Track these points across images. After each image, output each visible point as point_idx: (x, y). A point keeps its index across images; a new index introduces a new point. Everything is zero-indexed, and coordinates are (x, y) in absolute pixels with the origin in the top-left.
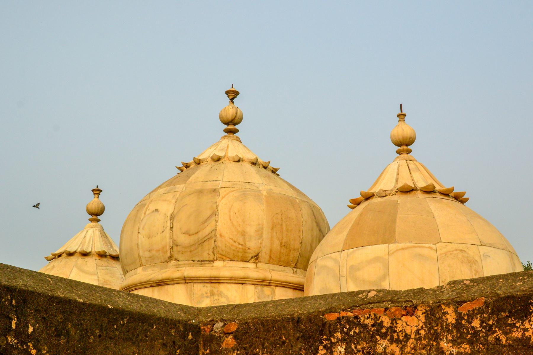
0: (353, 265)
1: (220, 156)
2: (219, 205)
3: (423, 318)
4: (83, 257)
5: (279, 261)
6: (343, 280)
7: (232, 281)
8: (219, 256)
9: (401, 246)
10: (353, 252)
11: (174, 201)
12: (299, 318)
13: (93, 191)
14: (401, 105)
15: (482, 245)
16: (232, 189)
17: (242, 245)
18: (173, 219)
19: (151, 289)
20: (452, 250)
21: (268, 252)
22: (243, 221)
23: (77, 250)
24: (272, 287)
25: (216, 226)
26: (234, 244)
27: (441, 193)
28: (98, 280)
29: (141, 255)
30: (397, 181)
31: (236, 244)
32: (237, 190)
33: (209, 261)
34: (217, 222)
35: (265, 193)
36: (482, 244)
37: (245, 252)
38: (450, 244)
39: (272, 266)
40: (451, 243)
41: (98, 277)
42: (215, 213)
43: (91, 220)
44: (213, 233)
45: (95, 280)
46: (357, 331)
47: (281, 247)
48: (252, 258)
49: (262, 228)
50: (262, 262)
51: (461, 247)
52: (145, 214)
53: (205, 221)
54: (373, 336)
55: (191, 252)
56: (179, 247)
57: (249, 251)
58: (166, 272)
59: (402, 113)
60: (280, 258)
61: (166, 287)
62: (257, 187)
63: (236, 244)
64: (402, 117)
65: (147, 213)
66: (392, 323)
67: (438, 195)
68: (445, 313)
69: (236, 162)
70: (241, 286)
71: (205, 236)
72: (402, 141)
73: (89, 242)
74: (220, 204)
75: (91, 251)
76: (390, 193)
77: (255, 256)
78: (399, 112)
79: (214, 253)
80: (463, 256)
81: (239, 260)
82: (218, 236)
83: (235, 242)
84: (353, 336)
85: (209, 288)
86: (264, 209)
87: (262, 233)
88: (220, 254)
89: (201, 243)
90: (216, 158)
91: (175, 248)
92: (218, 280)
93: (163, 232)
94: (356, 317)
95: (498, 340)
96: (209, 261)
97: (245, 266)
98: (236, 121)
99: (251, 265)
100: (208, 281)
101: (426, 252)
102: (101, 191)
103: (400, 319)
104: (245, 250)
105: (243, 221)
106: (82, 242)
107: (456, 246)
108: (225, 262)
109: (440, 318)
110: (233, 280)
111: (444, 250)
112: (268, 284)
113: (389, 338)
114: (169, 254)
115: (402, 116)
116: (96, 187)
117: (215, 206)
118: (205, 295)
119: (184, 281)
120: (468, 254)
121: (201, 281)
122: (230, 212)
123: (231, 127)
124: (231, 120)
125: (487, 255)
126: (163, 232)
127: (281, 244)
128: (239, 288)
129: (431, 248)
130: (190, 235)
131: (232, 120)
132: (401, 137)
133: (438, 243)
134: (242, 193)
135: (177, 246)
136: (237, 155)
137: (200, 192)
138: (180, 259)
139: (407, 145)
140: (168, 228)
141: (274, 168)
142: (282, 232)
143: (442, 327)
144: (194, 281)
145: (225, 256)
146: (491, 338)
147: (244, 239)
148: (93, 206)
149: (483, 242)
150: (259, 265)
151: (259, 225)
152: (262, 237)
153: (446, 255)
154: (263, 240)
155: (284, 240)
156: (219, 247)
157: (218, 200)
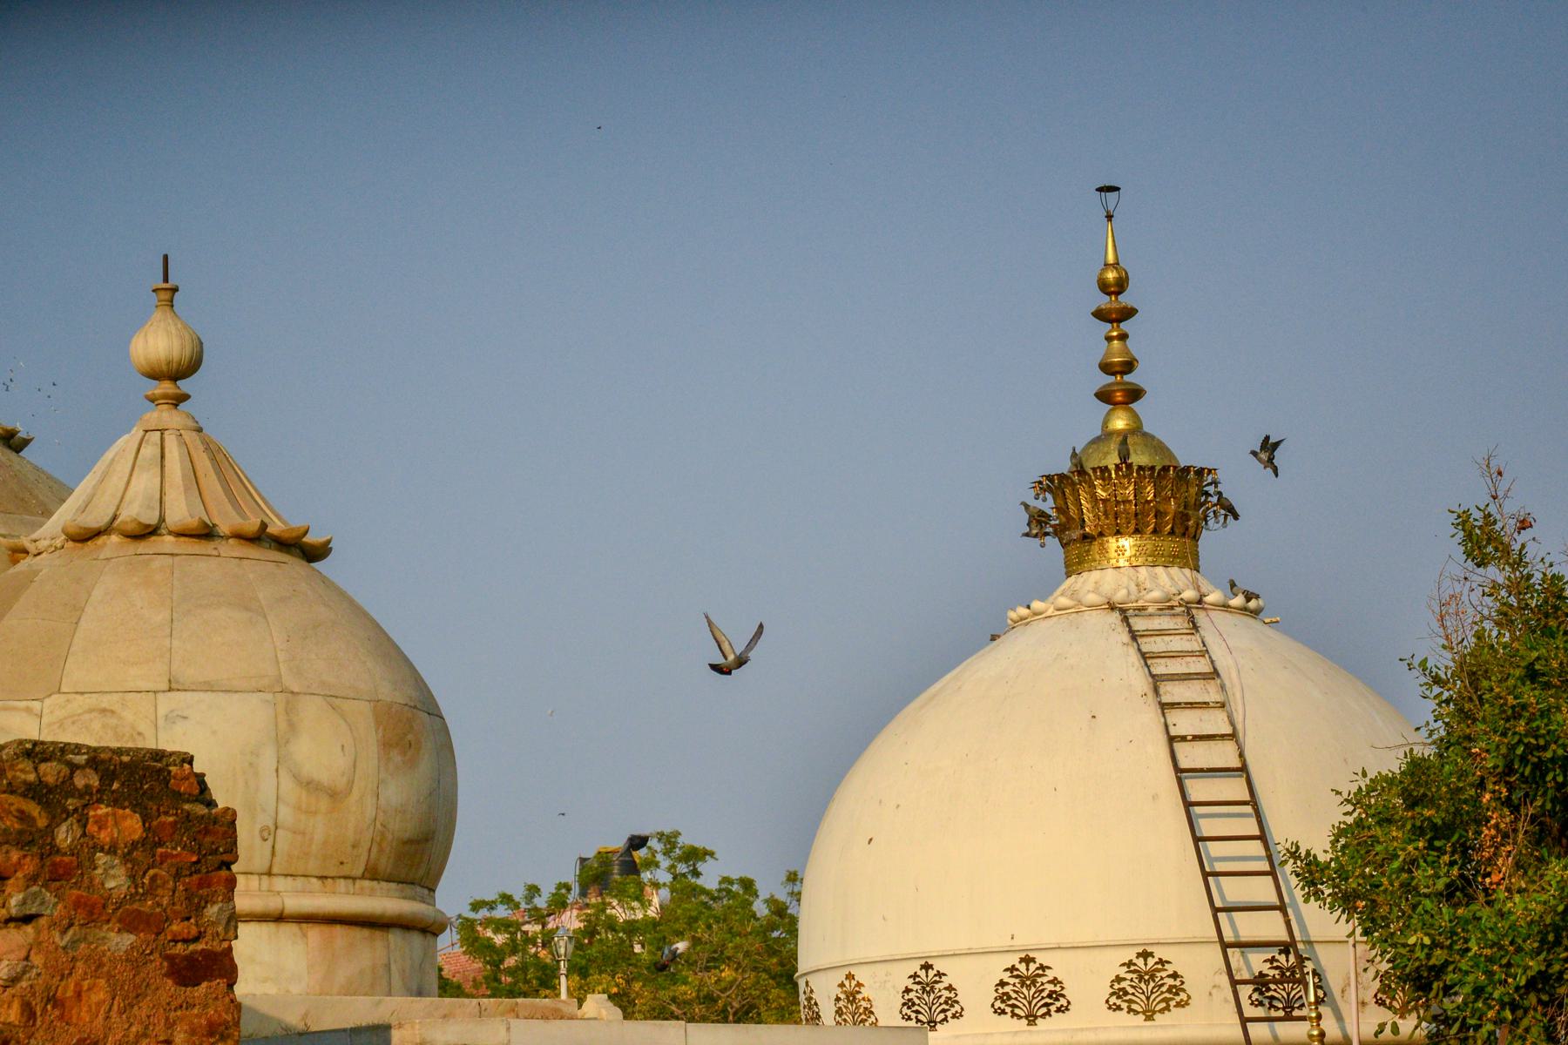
14: (166, 258)
15: (170, 690)
20: (79, 711)
36: (174, 686)
38: (78, 696)
40: (82, 693)
51: (105, 701)
72: (157, 370)
80: (104, 726)
107: (90, 700)
111: (60, 714)
120: (120, 718)
125: (178, 716)
129: (28, 710)
133: (50, 695)
149: (177, 682)
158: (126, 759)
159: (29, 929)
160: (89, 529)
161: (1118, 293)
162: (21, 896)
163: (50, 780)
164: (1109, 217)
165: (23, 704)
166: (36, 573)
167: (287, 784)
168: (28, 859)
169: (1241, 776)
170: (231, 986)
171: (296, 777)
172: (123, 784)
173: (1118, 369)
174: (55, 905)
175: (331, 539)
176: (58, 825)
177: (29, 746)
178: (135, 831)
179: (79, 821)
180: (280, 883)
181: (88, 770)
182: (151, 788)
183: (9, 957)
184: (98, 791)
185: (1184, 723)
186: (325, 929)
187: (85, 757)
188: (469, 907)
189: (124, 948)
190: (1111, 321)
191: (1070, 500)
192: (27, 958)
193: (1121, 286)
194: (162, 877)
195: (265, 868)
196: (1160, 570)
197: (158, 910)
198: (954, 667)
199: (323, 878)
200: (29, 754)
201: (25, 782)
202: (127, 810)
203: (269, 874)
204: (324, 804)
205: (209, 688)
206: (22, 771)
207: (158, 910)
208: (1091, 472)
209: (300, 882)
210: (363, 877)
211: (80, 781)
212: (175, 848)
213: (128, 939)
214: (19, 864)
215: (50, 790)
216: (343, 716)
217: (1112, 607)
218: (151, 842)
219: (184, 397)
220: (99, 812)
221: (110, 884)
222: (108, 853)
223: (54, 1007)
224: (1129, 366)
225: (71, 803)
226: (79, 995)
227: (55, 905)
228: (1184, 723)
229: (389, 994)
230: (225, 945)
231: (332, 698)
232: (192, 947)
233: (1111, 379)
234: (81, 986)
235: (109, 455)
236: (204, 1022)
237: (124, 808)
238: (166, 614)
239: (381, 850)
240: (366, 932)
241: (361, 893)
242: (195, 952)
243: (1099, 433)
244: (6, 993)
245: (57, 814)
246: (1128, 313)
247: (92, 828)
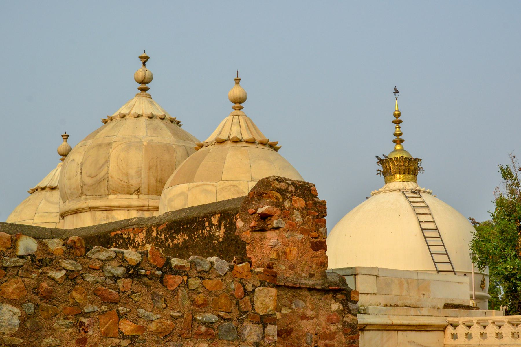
0: (170, 198)
1: (124, 114)
2: (110, 155)
3: (145, 234)
4: (51, 191)
5: (157, 192)
6: (166, 207)
7: (120, 209)
8: (112, 191)
9: (196, 184)
10: (172, 188)
11: (83, 153)
12: (100, 235)
13: (62, 136)
15: (252, 181)
16: (121, 142)
17: (126, 183)
18: (82, 166)
19: (72, 216)
21: (147, 187)
22: (127, 166)
23: (47, 185)
24: (151, 211)
25: (108, 170)
26: (121, 182)
27: (247, 142)
28: (60, 208)
29: (66, 191)
30: (220, 133)
31: (122, 183)
32: (125, 143)
33: (106, 195)
34: (108, 167)
35: (145, 143)
36: (253, 180)
37: (130, 188)
39: (151, 196)
40: (228, 181)
41: (60, 206)
42: (107, 161)
43: (234, 108)
44: (106, 175)
45: (57, 208)
46: (121, 242)
47: (156, 182)
48: (135, 191)
49: (141, 170)
50: (143, 194)
51: (234, 183)
52: (68, 162)
53: (101, 167)
54: (127, 245)
55: (93, 189)
56: (86, 186)
57: (132, 186)
58: (78, 204)
59: (237, 78)
60: (157, 190)
61: (80, 214)
62: (140, 139)
63: (122, 183)
64: (237, 81)
65: (69, 162)
66: (134, 237)
67: (244, 144)
68: (153, 231)
69: (136, 117)
70: (127, 212)
71: (101, 177)
73: (57, 179)
74: (112, 154)
75: (57, 186)
76: (211, 144)
77: (137, 190)
78: (236, 78)
79: (108, 190)
81: (126, 193)
82: (110, 177)
83: (121, 181)
84: (120, 245)
85: (105, 214)
86: (142, 156)
87: (141, 174)
88: (113, 190)
89: (99, 182)
90: (122, 116)
91: (84, 187)
92: (111, 208)
93: (76, 175)
94: (121, 234)
95: (169, 245)
96: (106, 195)
97: (130, 197)
98: (146, 81)
99: (135, 197)
100: (104, 209)
101: (209, 188)
102: (69, 136)
103: (138, 235)
104: (129, 186)
105: (127, 166)
106: (52, 178)
107: (231, 183)
108: (116, 196)
109: (151, 234)
110: (120, 208)
111: (222, 186)
112: (147, 209)
113: (132, 245)
114: (81, 191)
115: (238, 81)
116: (65, 133)
117: (107, 156)
118: (103, 219)
119: (89, 210)
121: (100, 210)
122: (117, 159)
123: (143, 86)
124: (141, 81)
126: (76, 175)
127: (156, 180)
128: (126, 213)
129: (213, 185)
130: (92, 177)
131: (143, 81)
132: (232, 98)
134: (127, 145)
135: (85, 185)
136: (135, 113)
137: (100, 145)
138: (88, 195)
139: (240, 103)
140: (79, 173)
141: (171, 118)
142: (157, 171)
143: (151, 239)
144: (96, 210)
145: (116, 191)
146: (167, 244)
147: (128, 179)
148: (62, 149)
149: (254, 179)
150: (141, 196)
151: (138, 168)
152: (141, 176)
153: (222, 189)
154: (142, 178)
155: (159, 177)
156: (111, 185)
157: (110, 151)
158: (300, 184)
159: (277, 231)
160: (223, 139)
161: (398, 117)
162: (276, 221)
163: (283, 188)
164: (396, 99)
165: (211, 183)
166: (209, 150)
168: (278, 210)
169: (436, 231)
170: (325, 251)
172: (300, 191)
173: (398, 135)
174: (284, 224)
175: (281, 147)
176: (285, 201)
177: (277, 177)
178: (303, 205)
179: (290, 200)
181: (292, 186)
182: (306, 193)
183: (273, 239)
184: (294, 192)
185: (422, 218)
187: (291, 182)
189: (301, 239)
190: (396, 124)
191: (387, 165)
192: (277, 240)
193: (399, 115)
194: (310, 219)
196: (409, 183)
197: (309, 228)
198: (358, 204)
200: (277, 180)
201: (277, 188)
202: (301, 198)
206: (276, 184)
207: (309, 228)
208: (393, 159)
211: (290, 189)
212: (312, 211)
213: (302, 236)
214: (276, 212)
215: (283, 191)
217: (399, 190)
218: (306, 208)
219: (242, 108)
220: (295, 198)
221: (297, 220)
222: (297, 210)
223: (284, 254)
224: (400, 134)
225: (289, 195)
226: (290, 251)
227: (284, 224)
228: (422, 218)
230: (324, 240)
232: (316, 240)
233: (397, 137)
234: (291, 249)
235: (224, 121)
236: (319, 262)
237: (301, 198)
238: (248, 161)
242: (317, 241)
243: (393, 150)
244: (272, 250)
245: (285, 198)
246: (401, 122)
247: (293, 203)
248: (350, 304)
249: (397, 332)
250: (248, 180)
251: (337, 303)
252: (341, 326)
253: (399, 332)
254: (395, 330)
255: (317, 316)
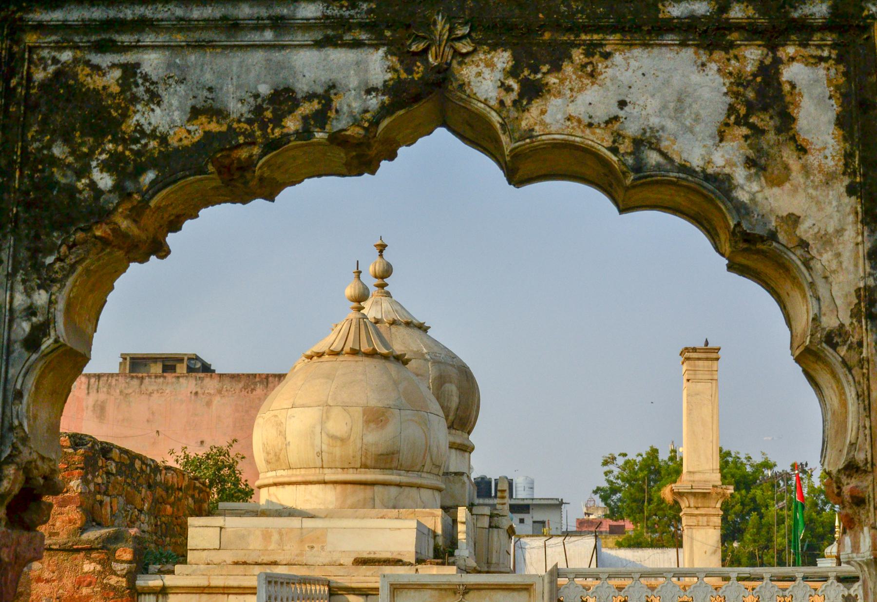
78: (356, 270)
167: (325, 437)
171: (328, 435)
180: (326, 471)
186: (344, 486)
188: (254, 492)
195: (320, 466)
199: (343, 469)
203: (322, 468)
204: (339, 443)
205: (303, 406)
209: (333, 470)
210: (361, 468)
216: (348, 413)
229: (374, 508)
231: (345, 407)
239: (367, 458)
240: (362, 487)
241: (360, 473)
248: (113, 564)
249: (226, 595)
250: (288, 407)
251: (93, 564)
252: (99, 589)
253: (231, 596)
254: (224, 594)
255: (60, 579)
